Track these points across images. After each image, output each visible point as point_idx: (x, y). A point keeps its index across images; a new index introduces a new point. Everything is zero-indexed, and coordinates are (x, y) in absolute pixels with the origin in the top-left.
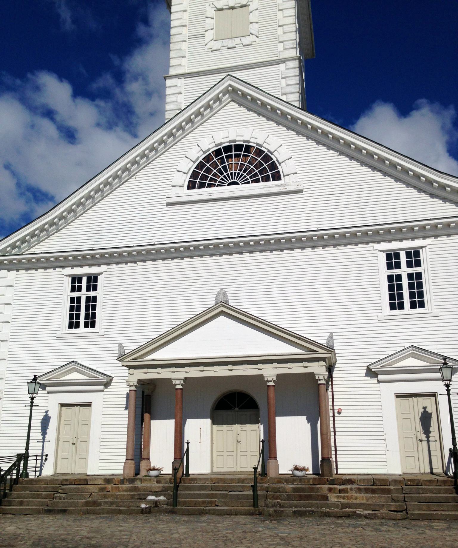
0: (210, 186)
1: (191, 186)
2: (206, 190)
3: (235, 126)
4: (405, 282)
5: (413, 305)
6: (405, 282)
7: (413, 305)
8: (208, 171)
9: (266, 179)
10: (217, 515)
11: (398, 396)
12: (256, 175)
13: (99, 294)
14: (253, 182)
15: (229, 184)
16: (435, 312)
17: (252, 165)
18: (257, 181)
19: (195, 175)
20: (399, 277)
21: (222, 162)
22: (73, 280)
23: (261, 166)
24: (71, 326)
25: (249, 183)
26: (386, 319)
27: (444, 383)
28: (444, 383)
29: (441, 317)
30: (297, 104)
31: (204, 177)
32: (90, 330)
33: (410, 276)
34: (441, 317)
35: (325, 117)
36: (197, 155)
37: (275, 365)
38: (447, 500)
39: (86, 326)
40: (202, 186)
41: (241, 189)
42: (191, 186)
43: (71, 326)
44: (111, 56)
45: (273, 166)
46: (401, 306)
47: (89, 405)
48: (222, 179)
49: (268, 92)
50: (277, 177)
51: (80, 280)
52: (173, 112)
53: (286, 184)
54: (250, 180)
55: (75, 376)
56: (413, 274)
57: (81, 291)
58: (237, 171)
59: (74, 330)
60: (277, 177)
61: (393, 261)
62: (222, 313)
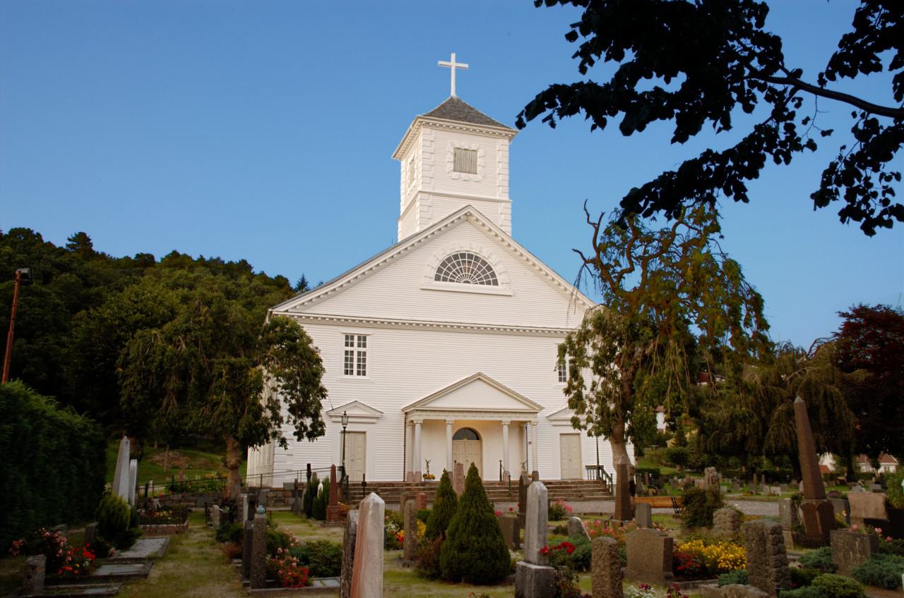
0: (451, 281)
1: (437, 278)
2: (448, 283)
7: (359, 373)
8: (449, 269)
9: (489, 283)
10: (280, 303)
12: (481, 279)
14: (480, 283)
15: (465, 282)
17: (440, 276)
18: (483, 283)
19: (439, 270)
21: (459, 265)
22: (347, 337)
24: (346, 372)
25: (477, 283)
30: (510, 234)
31: (447, 274)
32: (361, 377)
35: (818, 194)
37: (509, 415)
38: (599, 490)
39: (359, 373)
40: (445, 280)
41: (472, 287)
42: (437, 278)
43: (346, 372)
44: (97, 523)
45: (493, 275)
50: (496, 283)
52: (463, 201)
59: (348, 376)
60: (496, 283)
62: (479, 379)
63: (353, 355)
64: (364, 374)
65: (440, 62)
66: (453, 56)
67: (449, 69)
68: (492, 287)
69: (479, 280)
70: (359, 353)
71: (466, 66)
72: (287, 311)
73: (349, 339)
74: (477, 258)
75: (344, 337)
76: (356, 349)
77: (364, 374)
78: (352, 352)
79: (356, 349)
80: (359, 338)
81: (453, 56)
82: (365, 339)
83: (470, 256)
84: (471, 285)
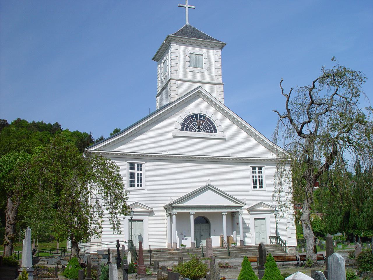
1: (182, 129)
3: (198, 107)
4: (136, 176)
5: (138, 186)
6: (136, 176)
7: (138, 186)
8: (189, 124)
9: (212, 132)
11: (256, 219)
13: (143, 172)
16: (146, 190)
19: (183, 124)
20: (134, 174)
23: (210, 126)
25: (205, 132)
26: (253, 192)
27: (130, 217)
28: (130, 217)
29: (268, 192)
32: (139, 188)
33: (138, 174)
34: (268, 192)
36: (185, 116)
40: (186, 130)
42: (182, 129)
46: (134, 186)
47: (142, 221)
48: (194, 128)
49: (214, 97)
50: (216, 131)
51: (134, 165)
53: (218, 135)
54: (206, 131)
55: (261, 208)
56: (139, 173)
57: (256, 173)
58: (204, 128)
60: (216, 131)
61: (139, 167)
72: (96, 150)
79: (136, 171)
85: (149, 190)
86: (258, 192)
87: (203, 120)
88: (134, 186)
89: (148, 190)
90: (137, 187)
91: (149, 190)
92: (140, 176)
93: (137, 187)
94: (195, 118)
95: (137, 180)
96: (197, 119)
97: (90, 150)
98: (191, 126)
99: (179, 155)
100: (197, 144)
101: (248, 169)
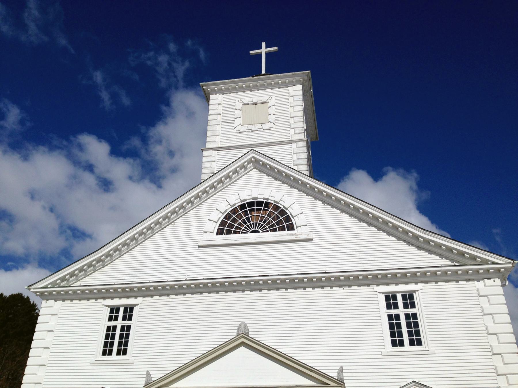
0: (235, 233)
1: (220, 232)
4: (403, 321)
5: (412, 343)
6: (403, 321)
7: (412, 343)
8: (234, 221)
9: (282, 229)
13: (133, 323)
14: (271, 231)
15: (252, 232)
18: (275, 230)
19: (223, 223)
25: (268, 231)
29: (437, 355)
30: (306, 173)
40: (229, 232)
41: (261, 236)
42: (220, 232)
43: (394, 344)
50: (291, 227)
53: (298, 233)
54: (269, 229)
58: (258, 222)
60: (291, 227)
62: (243, 344)
63: (399, 319)
64: (419, 343)
65: (251, 52)
66: (264, 44)
67: (260, 55)
68: (286, 232)
69: (269, 227)
70: (407, 316)
71: (275, 48)
72: (46, 287)
73: (391, 301)
74: (267, 204)
75: (383, 297)
76: (402, 311)
77: (419, 343)
78: (124, 319)
79: (402, 311)
80: (404, 297)
81: (264, 44)
82: (411, 297)
83: (259, 203)
84: (261, 234)
85: (137, 360)
86: (115, 363)
87: (264, 209)
88: (402, 344)
89: (135, 361)
90: (410, 345)
91: (137, 360)
92: (413, 320)
93: (410, 345)
94: (248, 209)
95: (406, 330)
96: (252, 211)
97: (34, 289)
98: (240, 224)
99: (132, 283)
100: (258, 254)
101: (375, 296)
